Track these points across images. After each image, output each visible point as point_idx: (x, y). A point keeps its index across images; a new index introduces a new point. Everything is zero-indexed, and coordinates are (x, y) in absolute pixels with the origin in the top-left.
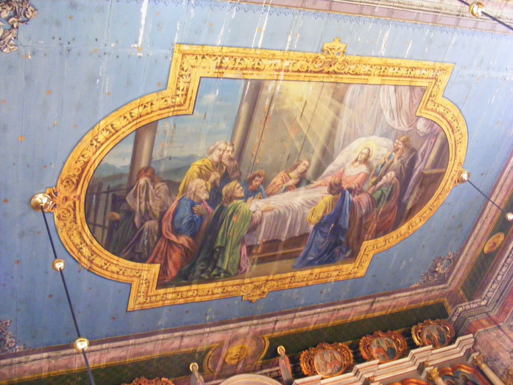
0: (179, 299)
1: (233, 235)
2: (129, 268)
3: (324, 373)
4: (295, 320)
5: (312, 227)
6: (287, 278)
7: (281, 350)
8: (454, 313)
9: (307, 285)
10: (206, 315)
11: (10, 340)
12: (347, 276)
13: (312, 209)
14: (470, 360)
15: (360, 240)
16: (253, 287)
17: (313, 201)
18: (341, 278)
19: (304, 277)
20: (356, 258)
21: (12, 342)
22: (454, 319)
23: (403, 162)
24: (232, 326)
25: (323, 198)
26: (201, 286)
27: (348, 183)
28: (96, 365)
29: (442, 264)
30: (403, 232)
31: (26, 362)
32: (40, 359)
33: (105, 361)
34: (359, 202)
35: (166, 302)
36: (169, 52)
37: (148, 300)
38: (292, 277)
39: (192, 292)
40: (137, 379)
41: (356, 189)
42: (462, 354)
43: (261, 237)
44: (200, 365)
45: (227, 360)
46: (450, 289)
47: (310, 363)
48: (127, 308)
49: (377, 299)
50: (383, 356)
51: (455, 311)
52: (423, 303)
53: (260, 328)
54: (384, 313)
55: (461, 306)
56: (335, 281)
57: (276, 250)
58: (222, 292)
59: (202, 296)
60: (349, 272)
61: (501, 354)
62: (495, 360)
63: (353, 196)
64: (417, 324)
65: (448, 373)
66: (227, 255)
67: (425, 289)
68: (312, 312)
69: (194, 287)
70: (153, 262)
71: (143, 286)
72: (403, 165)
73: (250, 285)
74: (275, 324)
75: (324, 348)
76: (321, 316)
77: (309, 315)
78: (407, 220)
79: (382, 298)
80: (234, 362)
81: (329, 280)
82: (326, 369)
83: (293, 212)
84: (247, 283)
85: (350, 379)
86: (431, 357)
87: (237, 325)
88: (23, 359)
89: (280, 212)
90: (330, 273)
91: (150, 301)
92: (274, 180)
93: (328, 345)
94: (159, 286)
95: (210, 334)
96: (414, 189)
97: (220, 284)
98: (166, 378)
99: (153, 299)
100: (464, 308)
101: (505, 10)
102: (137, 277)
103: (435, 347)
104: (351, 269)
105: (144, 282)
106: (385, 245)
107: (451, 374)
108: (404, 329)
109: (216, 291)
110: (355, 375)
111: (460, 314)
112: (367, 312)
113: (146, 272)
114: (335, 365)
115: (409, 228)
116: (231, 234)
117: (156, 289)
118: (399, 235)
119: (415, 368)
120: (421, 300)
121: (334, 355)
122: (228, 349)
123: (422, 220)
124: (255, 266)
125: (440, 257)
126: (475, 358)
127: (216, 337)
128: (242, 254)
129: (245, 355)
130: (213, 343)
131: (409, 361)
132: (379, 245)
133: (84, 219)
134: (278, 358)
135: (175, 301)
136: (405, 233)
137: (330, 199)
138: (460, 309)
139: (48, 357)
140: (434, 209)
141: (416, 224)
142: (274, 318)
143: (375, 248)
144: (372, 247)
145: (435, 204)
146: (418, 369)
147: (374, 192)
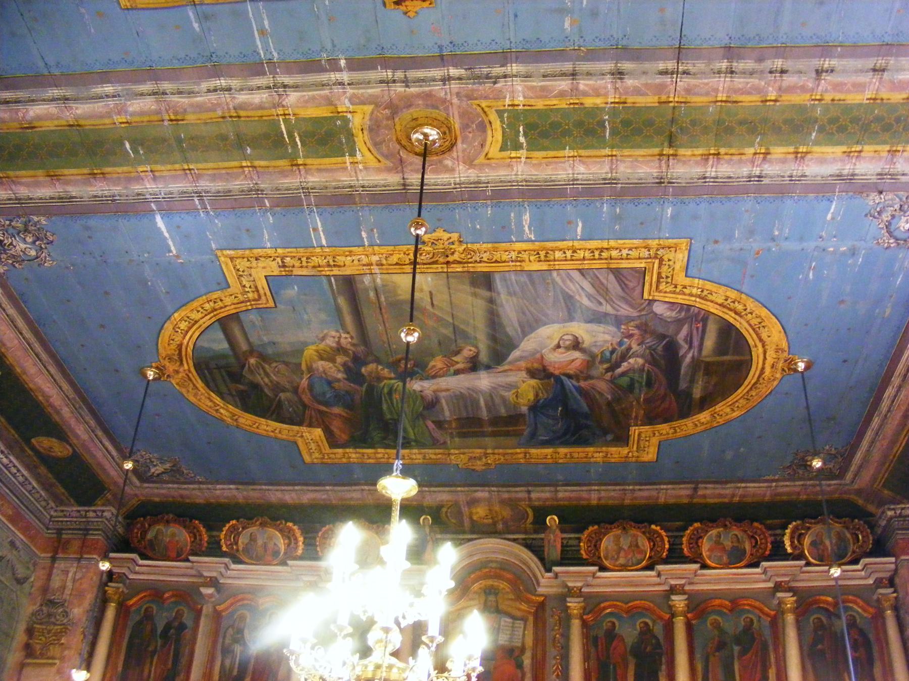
36: (213, 257)
55: (893, 509)
82: (618, 557)
85: (650, 579)
92: (432, 363)
100: (898, 512)
101: (766, 166)
119: (771, 585)
121: (637, 540)
133: (206, 388)
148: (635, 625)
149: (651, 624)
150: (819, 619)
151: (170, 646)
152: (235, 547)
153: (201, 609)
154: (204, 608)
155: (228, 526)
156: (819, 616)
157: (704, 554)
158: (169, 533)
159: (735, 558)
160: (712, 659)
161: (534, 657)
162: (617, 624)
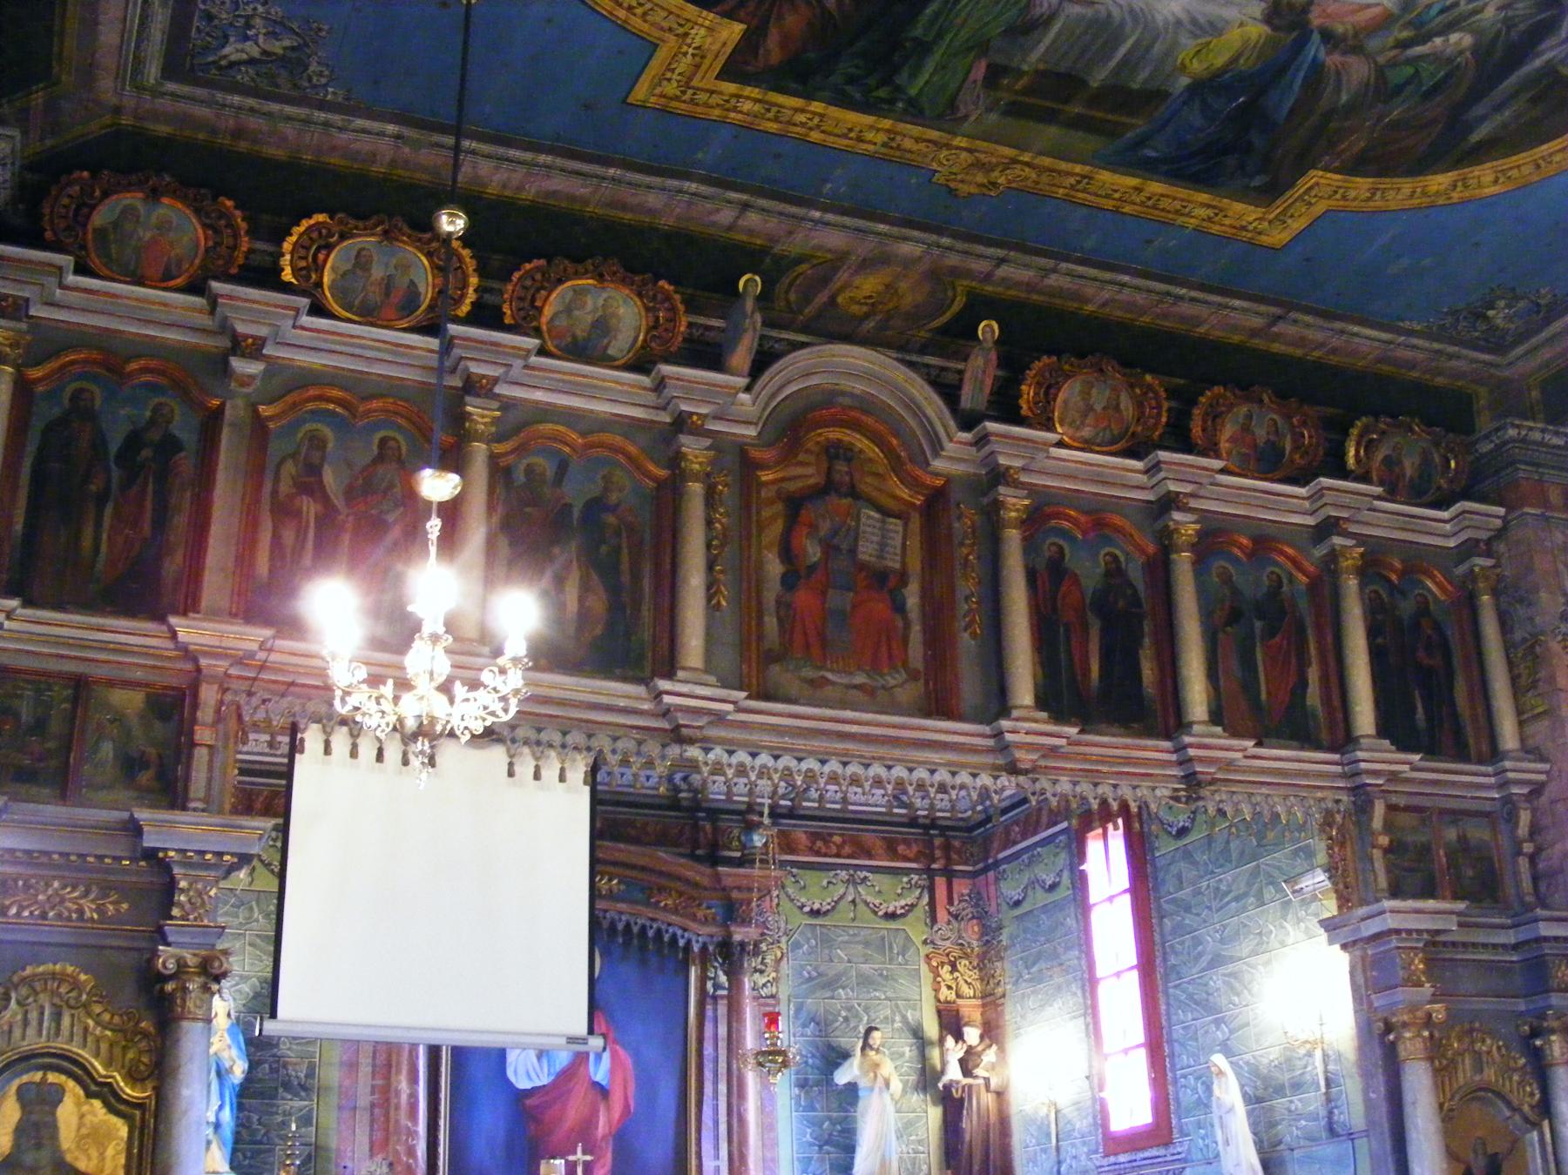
0: (769, 119)
1: (963, 25)
2: (663, 8)
3: (1071, 432)
4: (1054, 276)
5: (1184, 81)
6: (1069, 174)
7: (988, 329)
8: (1490, 432)
9: (1116, 211)
10: (825, 181)
11: (320, 68)
12: (1234, 231)
13: (1200, 41)
14: (1461, 570)
15: (1303, 163)
16: (970, 161)
17: (1211, 23)
18: (1215, 229)
19: (1115, 187)
20: (1274, 201)
21: (321, 74)
22: (1485, 447)
23: (1509, 24)
24: (882, 227)
25: (1241, 25)
26: (834, 112)
27: (1329, 16)
28: (507, 193)
29: (1509, 306)
30: (1434, 188)
31: (340, 129)
32: (377, 134)
33: (533, 191)
34: (1338, 73)
35: (732, 115)
37: (687, 97)
38: (1084, 177)
39: (808, 116)
40: (599, 259)
41: (1344, 38)
42: (1452, 543)
43: (1035, 56)
44: (769, 284)
45: (840, 300)
46: (1507, 373)
47: (1049, 391)
48: (627, 97)
49: (1293, 315)
50: (1245, 455)
51: (1497, 430)
52: (1415, 374)
53: (953, 260)
54: (1299, 352)
55: (1518, 427)
56: (1194, 229)
57: (1066, 101)
58: (884, 145)
59: (830, 134)
60: (1244, 223)
61: (1544, 595)
62: (1521, 601)
63: (1329, 53)
64: (1376, 415)
65: (1385, 573)
66: (930, 65)
67: (1436, 346)
68: (1108, 276)
69: (817, 106)
70: (730, 15)
71: (684, 60)
72: (1509, 29)
73: (964, 155)
74: (998, 266)
75: (1101, 370)
76: (1126, 294)
77: (1095, 279)
78: (1458, 164)
79: (1309, 319)
80: (855, 309)
81: (1180, 220)
82: (1082, 423)
83: (1144, 29)
84: (958, 148)
86: (1366, 515)
87: (895, 230)
88: (336, 118)
89: (1109, 15)
90: (1191, 206)
91: (692, 100)
93: (1117, 366)
94: (725, 75)
95: (820, 226)
96: (1514, 95)
97: (886, 123)
98: (670, 283)
99: (702, 97)
102: (677, 35)
103: (1391, 496)
104: (1251, 219)
105: (691, 51)
106: (1369, 199)
107: (1394, 577)
108: (1340, 411)
109: (870, 136)
110: (1146, 472)
111: (1505, 443)
112: (1254, 333)
113: (703, 32)
114: (1109, 426)
115: (1455, 187)
116: (959, 21)
117: (716, 78)
118: (1419, 190)
119: (1310, 521)
120: (1413, 366)
121: (1118, 397)
122: (852, 275)
123: (1501, 181)
124: (993, 117)
125: (1513, 289)
126: (1477, 569)
127: (835, 240)
128: (971, 77)
129: (891, 306)
130: (820, 247)
131: (1303, 498)
132: (1352, 194)
134: (971, 343)
135: (757, 121)
136: (1437, 194)
137: (1260, 36)
138: (1512, 432)
139: (398, 137)
140: (1548, 170)
141: (1480, 186)
142: (1000, 253)
143: (1338, 196)
144: (1329, 190)
145: (1557, 158)
146: (1317, 526)
147: (1393, 64)
148: (1097, 554)
149: (1122, 559)
150: (1376, 592)
151: (146, 484)
152: (314, 276)
153: (221, 409)
154: (228, 406)
155: (305, 224)
156: (1375, 587)
157: (1222, 445)
158: (154, 220)
159: (1268, 462)
160: (1221, 636)
161: (925, 594)
162: (1067, 551)
